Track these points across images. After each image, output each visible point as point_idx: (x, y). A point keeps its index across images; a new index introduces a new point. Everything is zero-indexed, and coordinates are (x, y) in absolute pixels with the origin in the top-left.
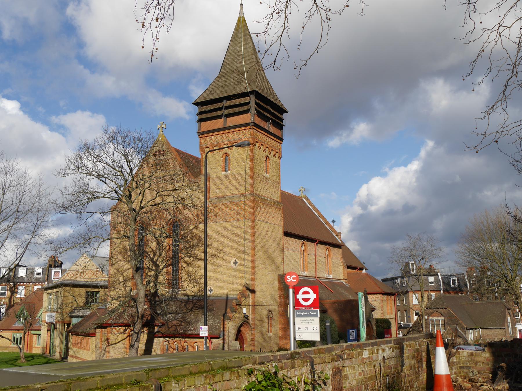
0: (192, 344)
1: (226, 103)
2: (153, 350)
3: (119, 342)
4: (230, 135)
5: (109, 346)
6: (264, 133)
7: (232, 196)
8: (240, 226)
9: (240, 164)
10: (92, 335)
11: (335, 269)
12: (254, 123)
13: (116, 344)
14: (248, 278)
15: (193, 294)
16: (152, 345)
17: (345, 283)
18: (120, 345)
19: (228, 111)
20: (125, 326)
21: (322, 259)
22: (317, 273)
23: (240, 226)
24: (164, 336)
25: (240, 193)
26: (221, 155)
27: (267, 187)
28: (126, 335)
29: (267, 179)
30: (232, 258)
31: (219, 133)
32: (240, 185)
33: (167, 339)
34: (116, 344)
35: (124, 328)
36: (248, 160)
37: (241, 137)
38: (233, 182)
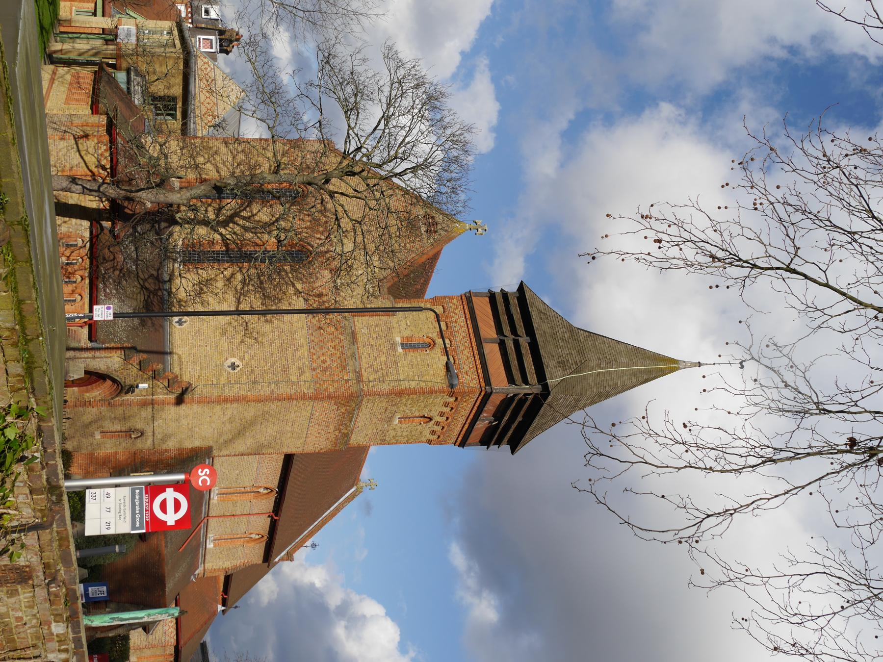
0: (78, 291)
1: (524, 341)
2: (67, 219)
3: (82, 157)
4: (467, 350)
5: (75, 138)
7: (357, 356)
8: (301, 372)
9: (415, 370)
10: (95, 108)
11: (225, 553)
12: (491, 393)
13: (79, 151)
14: (204, 391)
15: (174, 290)
16: (76, 218)
17: (197, 572)
18: (76, 159)
19: (510, 345)
20: (111, 168)
21: (243, 528)
22: (215, 520)
23: (301, 372)
24: (94, 239)
25: (363, 371)
26: (430, 335)
30: (242, 359)
31: (471, 331)
32: (377, 371)
33: (88, 245)
34: (79, 151)
35: (108, 166)
36: (423, 385)
38: (383, 358)
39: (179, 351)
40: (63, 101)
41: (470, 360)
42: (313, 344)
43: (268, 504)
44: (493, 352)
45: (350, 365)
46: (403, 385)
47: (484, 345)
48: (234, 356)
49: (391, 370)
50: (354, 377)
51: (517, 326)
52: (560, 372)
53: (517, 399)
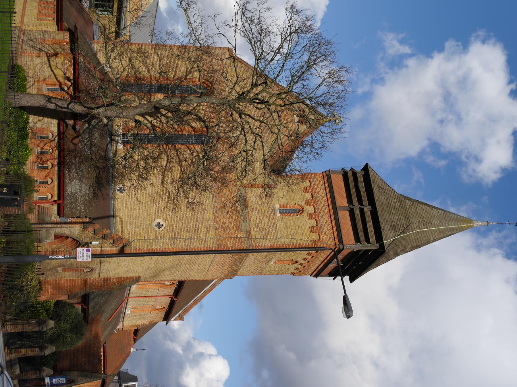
0: (51, 175)
1: (367, 209)
2: (41, 118)
3: (52, 71)
4: (327, 215)
5: (47, 56)
6: (328, 258)
7: (247, 219)
8: (208, 231)
9: (289, 230)
10: (60, 27)
12: (343, 249)
13: (50, 66)
14: (138, 244)
15: (111, 155)
16: (48, 117)
17: (118, 328)
18: (48, 72)
19: (357, 212)
20: (74, 79)
21: (152, 303)
23: (208, 231)
24: (61, 134)
25: (252, 230)
26: (300, 203)
27: (257, 262)
28: (61, 79)
29: (268, 262)
30: (166, 220)
31: (330, 201)
32: (262, 231)
33: (57, 139)
34: (50, 66)
35: (72, 78)
36: (294, 241)
37: (324, 231)
38: (266, 220)
39: (119, 213)
40: (36, 16)
41: (328, 223)
42: (216, 209)
43: (171, 291)
44: (344, 217)
45: (242, 228)
46: (280, 241)
47: (338, 211)
48: (159, 218)
49: (271, 230)
50: (245, 236)
51: (363, 199)
52: (392, 234)
53: (360, 253)
